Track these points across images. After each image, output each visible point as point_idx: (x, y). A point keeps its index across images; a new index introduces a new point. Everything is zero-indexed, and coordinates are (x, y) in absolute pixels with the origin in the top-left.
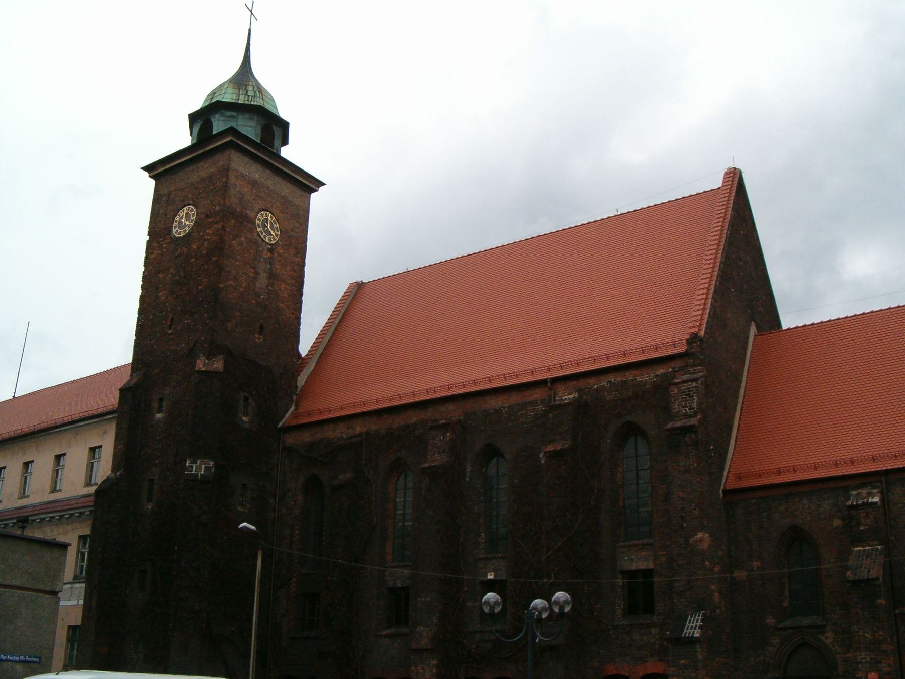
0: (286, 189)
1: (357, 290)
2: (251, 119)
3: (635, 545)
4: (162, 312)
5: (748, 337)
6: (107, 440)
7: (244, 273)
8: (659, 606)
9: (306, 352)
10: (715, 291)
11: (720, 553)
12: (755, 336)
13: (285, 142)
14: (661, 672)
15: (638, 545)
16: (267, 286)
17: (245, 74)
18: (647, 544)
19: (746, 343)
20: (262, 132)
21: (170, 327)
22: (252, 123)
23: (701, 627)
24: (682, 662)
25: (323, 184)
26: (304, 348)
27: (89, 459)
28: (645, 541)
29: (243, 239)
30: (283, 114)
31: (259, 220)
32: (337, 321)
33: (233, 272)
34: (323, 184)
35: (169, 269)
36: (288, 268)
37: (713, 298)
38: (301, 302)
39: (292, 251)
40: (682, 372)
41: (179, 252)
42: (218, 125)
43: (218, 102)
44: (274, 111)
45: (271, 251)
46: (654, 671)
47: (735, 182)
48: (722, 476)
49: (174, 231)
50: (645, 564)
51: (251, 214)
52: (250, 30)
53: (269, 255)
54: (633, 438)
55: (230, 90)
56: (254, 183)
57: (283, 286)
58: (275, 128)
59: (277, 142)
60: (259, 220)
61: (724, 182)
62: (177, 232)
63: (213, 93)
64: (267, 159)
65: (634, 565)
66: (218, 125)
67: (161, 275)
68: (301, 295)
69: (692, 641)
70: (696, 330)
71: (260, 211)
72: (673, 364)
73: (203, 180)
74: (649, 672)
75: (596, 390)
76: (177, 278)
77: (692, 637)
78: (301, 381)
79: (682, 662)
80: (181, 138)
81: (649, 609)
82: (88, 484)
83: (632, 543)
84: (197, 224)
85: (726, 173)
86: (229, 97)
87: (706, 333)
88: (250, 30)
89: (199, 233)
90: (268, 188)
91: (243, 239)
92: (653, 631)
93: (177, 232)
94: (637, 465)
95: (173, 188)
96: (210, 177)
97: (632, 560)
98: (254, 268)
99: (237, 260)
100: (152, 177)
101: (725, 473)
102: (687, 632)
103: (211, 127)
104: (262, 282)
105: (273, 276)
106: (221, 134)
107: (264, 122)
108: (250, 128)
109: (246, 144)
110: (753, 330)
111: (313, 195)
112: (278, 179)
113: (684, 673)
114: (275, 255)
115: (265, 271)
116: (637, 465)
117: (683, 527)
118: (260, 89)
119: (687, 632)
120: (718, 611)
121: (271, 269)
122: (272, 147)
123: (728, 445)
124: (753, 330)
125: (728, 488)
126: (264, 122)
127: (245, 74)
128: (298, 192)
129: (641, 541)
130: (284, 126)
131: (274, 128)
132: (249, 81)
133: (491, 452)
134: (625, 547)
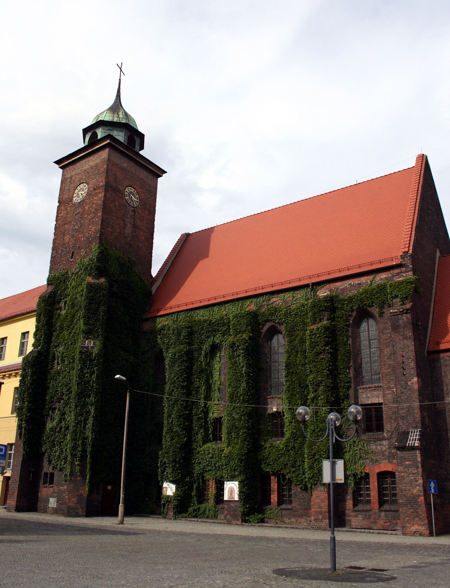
0: (143, 174)
1: (186, 239)
2: (121, 131)
3: (369, 388)
4: (66, 248)
5: (436, 258)
6: (30, 325)
7: (117, 224)
8: (387, 426)
9: (156, 275)
10: (416, 227)
11: (427, 392)
12: (439, 257)
13: (142, 148)
14: (391, 470)
15: (372, 387)
16: (132, 233)
17: (117, 106)
18: (378, 387)
19: (435, 261)
20: (128, 140)
21: (72, 258)
22: (122, 134)
23: (419, 440)
24: (407, 463)
25: (165, 172)
26: (154, 272)
27: (21, 339)
28: (377, 385)
29: (117, 203)
30: (141, 129)
31: (127, 192)
32: (174, 256)
33: (111, 223)
34: (165, 172)
35: (70, 222)
36: (144, 222)
37: (415, 231)
38: (152, 243)
39: (147, 212)
40: (398, 277)
41: (77, 212)
42: (100, 133)
43: (100, 120)
44: (136, 128)
45: (134, 211)
46: (386, 469)
47: (424, 163)
48: (426, 342)
49: (74, 199)
50: (377, 399)
51: (121, 188)
52: (120, 80)
53: (133, 213)
54: (366, 319)
55: (108, 115)
56: (123, 169)
57: (141, 233)
58: (136, 137)
59: (137, 147)
60: (127, 192)
61: (416, 162)
62: (76, 200)
63: (98, 116)
64: (131, 155)
65: (370, 400)
66: (100, 133)
67: (66, 226)
68: (153, 239)
69: (413, 448)
70: (407, 249)
71: (127, 186)
72: (392, 272)
73: (92, 168)
74: (382, 470)
75: (342, 289)
76: (76, 227)
77: (414, 446)
78: (154, 289)
79: (407, 463)
80: (78, 142)
81: (380, 428)
82: (21, 352)
83: (368, 386)
84: (88, 194)
85: (417, 158)
86: (108, 117)
87: (412, 252)
88: (120, 80)
89: (89, 199)
90: (132, 173)
91: (117, 203)
92: (384, 443)
93: (76, 200)
94: (369, 338)
95: (73, 173)
96: (96, 165)
97: (368, 397)
98: (124, 221)
99: (113, 216)
100: (60, 167)
101: (427, 341)
102: (410, 443)
103: (97, 136)
104: (129, 230)
105: (135, 226)
106: (103, 139)
107: (129, 134)
108: (120, 136)
109: (120, 146)
110: (438, 254)
111: (159, 179)
112: (138, 168)
113: (408, 470)
114: (137, 214)
115: (130, 223)
116: (369, 338)
117: (404, 375)
118: (126, 114)
119: (410, 443)
120: (428, 429)
121: (134, 222)
122: (134, 148)
123: (428, 324)
124: (438, 254)
125: (430, 350)
126: (129, 134)
127: (117, 106)
128: (150, 176)
129: (374, 385)
130: (142, 136)
131: (135, 137)
132: (120, 109)
133: (274, 331)
134: (363, 388)
